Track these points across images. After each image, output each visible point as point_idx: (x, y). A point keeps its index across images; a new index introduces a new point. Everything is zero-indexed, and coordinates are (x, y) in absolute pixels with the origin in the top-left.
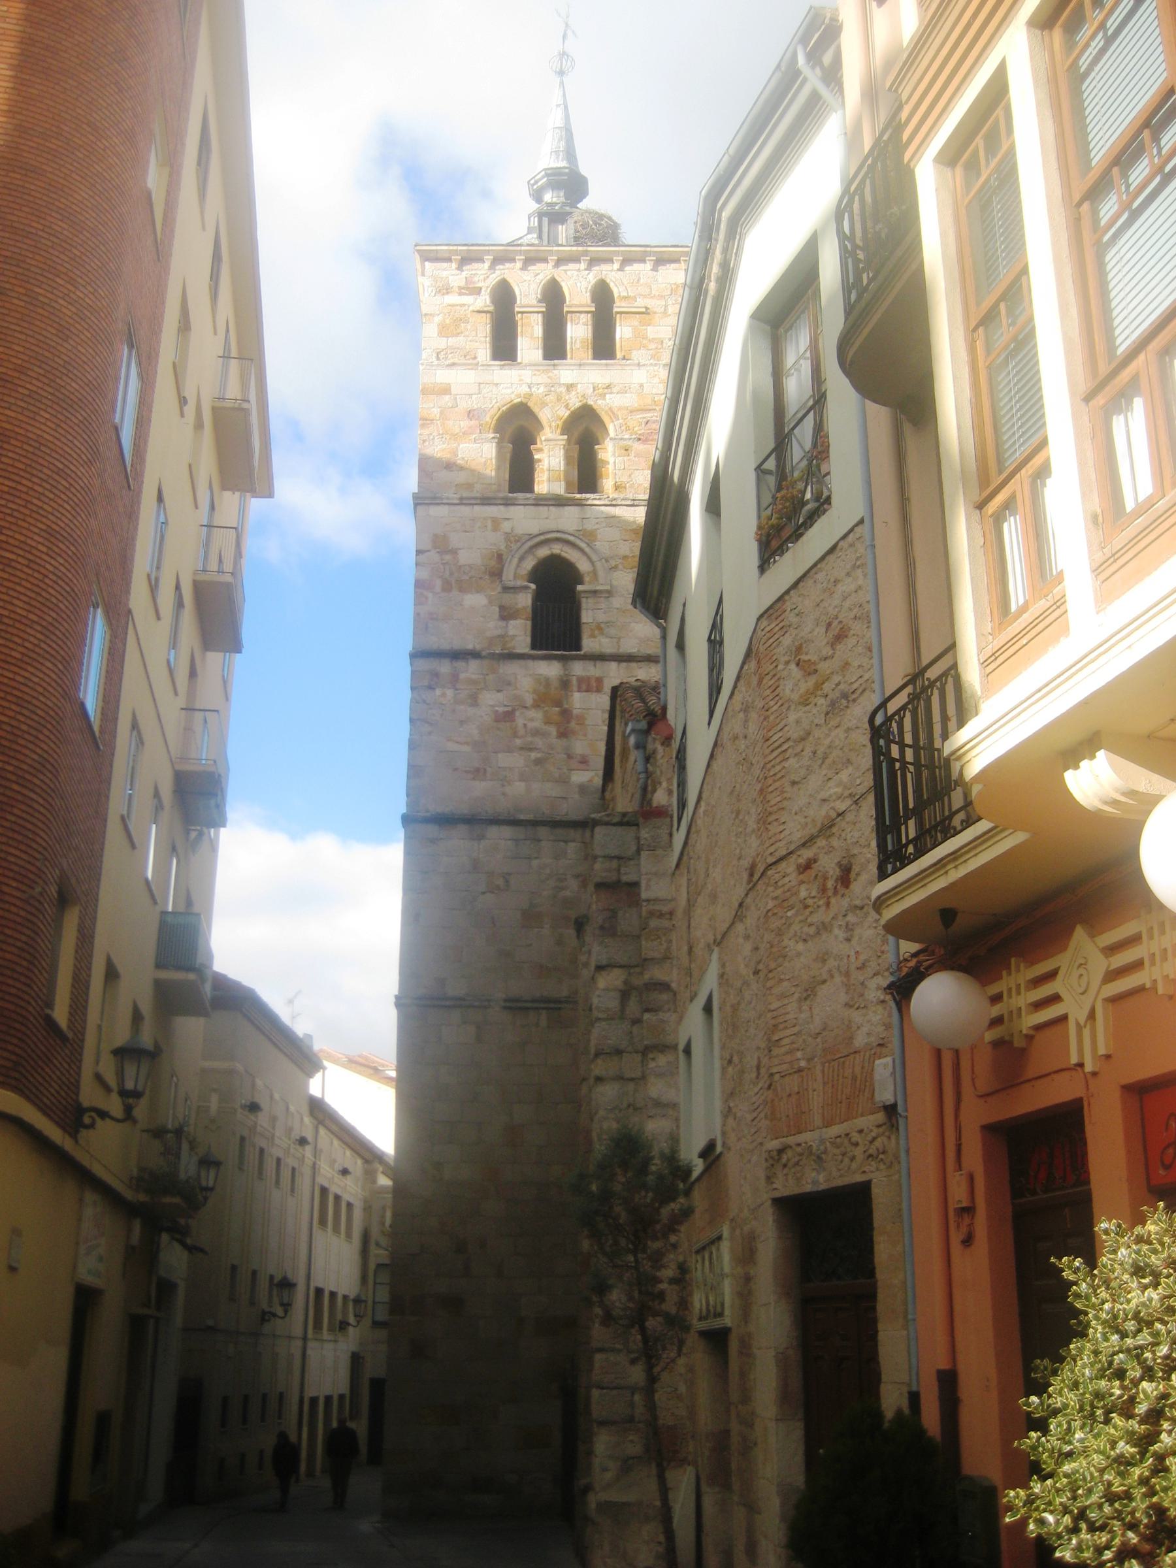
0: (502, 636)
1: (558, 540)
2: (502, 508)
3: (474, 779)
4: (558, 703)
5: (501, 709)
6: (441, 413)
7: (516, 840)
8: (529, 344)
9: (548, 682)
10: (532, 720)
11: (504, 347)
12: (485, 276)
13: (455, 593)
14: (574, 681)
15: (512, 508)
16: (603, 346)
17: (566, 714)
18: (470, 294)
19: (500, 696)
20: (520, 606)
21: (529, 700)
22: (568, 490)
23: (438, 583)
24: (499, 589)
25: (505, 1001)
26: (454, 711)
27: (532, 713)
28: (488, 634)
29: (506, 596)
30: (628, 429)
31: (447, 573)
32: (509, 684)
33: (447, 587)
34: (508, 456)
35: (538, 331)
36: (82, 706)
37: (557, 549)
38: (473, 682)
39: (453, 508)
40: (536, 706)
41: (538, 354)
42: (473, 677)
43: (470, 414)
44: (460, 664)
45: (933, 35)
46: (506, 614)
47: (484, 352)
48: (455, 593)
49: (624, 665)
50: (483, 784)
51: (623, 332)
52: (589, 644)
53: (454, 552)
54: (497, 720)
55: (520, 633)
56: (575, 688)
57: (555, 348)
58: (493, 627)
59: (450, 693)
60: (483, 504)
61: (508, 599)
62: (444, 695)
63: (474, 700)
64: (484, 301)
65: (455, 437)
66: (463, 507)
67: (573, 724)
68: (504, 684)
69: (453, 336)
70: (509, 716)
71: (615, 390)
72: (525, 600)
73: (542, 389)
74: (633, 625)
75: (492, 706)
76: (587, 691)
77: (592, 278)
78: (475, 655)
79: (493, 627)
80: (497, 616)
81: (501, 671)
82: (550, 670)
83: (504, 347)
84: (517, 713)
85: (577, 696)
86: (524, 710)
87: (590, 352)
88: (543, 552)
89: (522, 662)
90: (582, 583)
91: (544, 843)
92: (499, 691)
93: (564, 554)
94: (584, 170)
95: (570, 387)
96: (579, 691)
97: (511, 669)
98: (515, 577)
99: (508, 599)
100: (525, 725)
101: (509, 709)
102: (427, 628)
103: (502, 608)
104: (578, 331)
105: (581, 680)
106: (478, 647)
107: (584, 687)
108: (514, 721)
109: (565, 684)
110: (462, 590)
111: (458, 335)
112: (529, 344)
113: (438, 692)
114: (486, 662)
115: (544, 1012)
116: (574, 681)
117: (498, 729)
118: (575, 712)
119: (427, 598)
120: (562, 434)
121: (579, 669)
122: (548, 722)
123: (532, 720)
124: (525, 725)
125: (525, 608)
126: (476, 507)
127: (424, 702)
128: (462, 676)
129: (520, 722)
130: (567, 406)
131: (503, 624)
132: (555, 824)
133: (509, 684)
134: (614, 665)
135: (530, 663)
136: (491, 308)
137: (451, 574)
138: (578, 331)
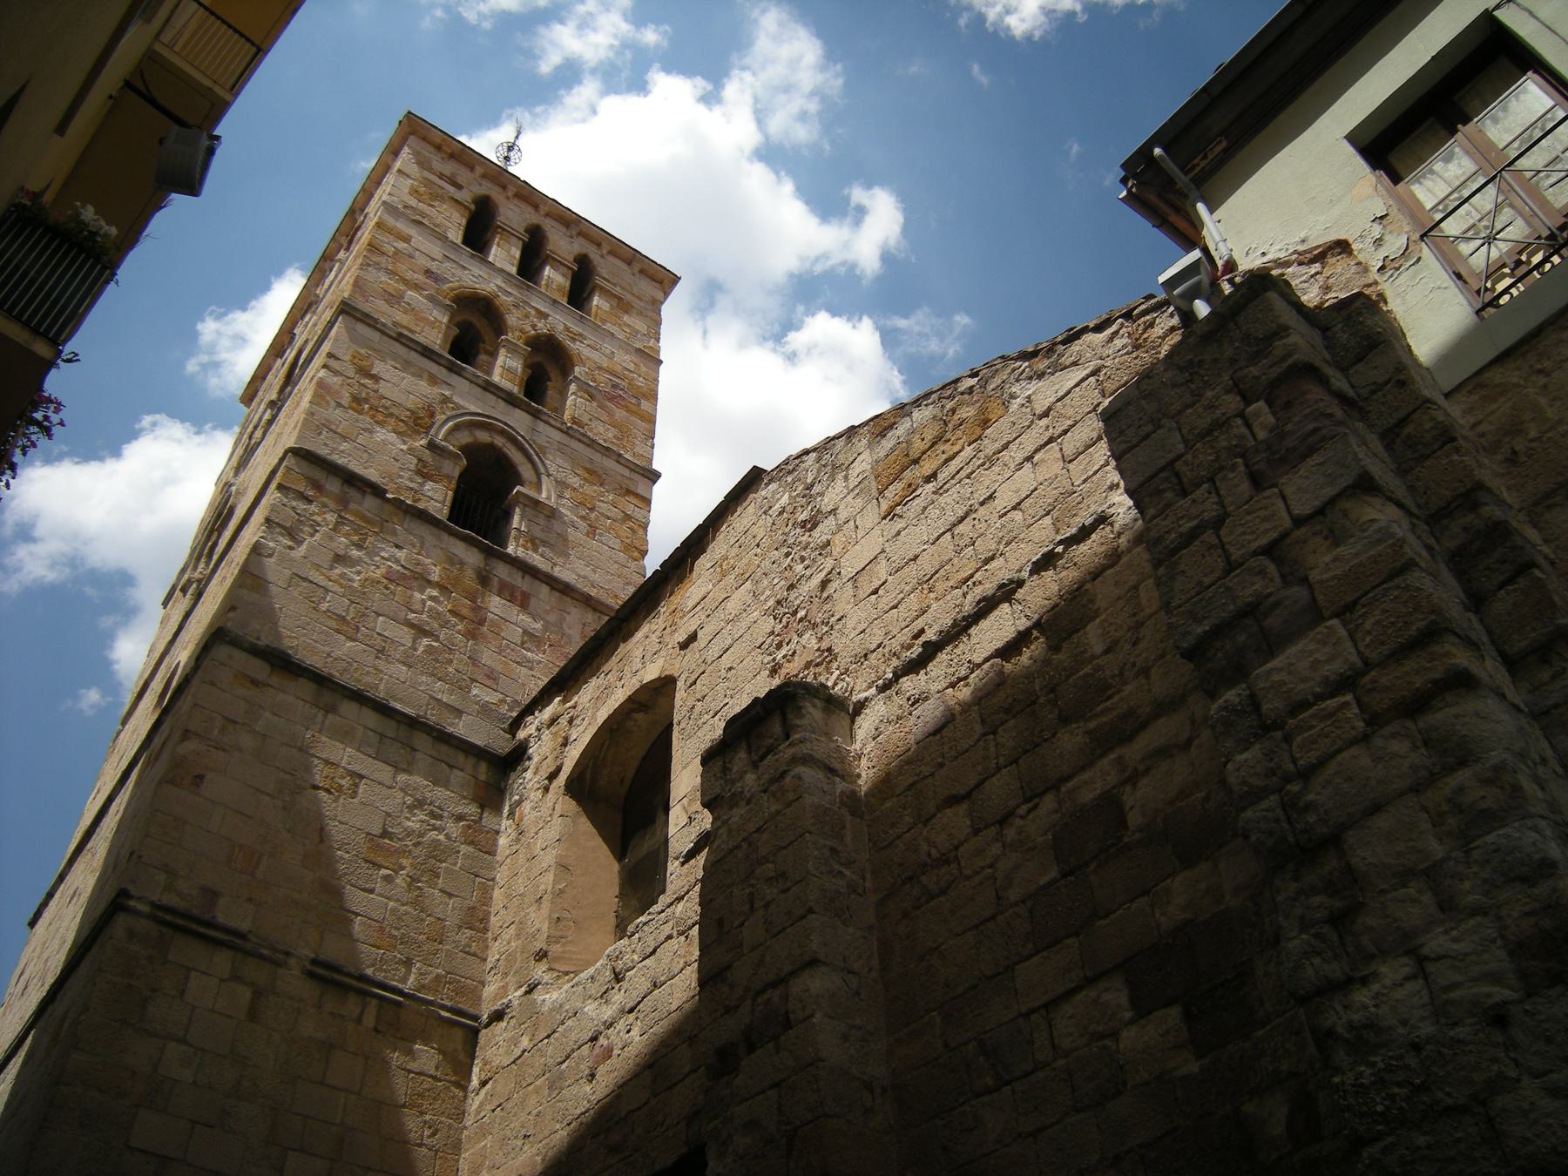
2: (444, 371)
7: (382, 736)
14: (495, 581)
25: (314, 962)
37: (499, 441)
46: (424, 473)
47: (456, 235)
55: (437, 498)
66: (397, 345)
78: (377, 491)
91: (419, 755)
98: (445, 439)
114: (388, 507)
115: (374, 1002)
134: (545, 589)
135: (445, 536)
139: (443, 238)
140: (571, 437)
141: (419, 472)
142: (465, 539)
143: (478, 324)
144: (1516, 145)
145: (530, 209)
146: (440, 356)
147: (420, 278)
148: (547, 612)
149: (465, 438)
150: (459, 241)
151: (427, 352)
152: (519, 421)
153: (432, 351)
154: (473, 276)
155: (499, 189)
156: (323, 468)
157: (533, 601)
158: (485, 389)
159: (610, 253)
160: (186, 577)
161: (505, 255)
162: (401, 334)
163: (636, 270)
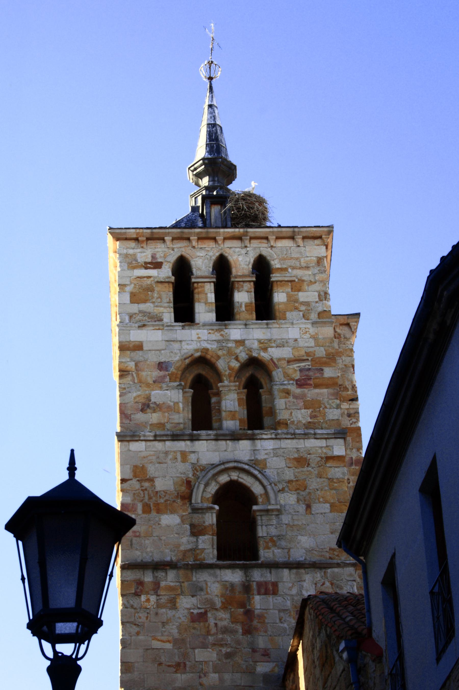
3: (176, 672)
4: (243, 605)
37: (234, 476)
40: (224, 607)
47: (169, 316)
50: (184, 676)
53: (151, 480)
74: (299, 537)
92: (193, 596)
93: (241, 480)
113: (143, 598)
114: (181, 572)
134: (286, 572)
152: (242, 450)
161: (205, 311)
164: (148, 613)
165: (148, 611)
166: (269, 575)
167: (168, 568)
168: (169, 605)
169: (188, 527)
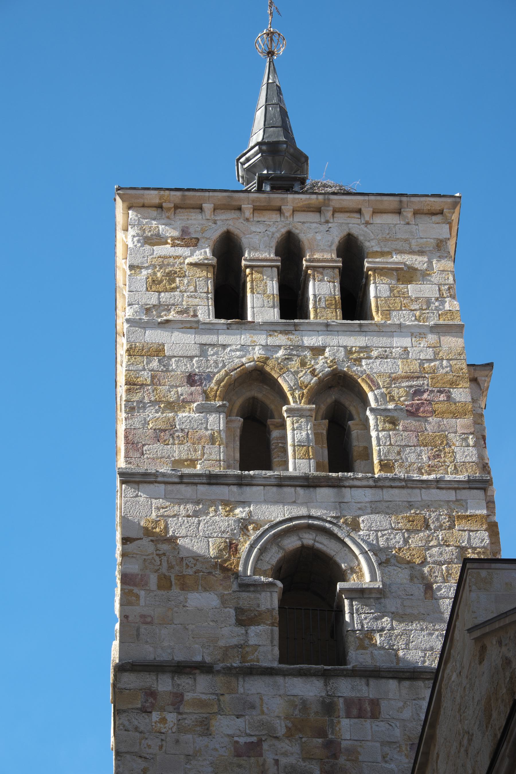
0: (241, 646)
1: (310, 527)
2: (234, 489)
4: (321, 733)
5: (242, 740)
6: (153, 377)
8: (261, 300)
9: (304, 705)
10: (285, 754)
11: (229, 303)
12: (212, 226)
13: (176, 590)
14: (341, 703)
15: (248, 489)
16: (353, 305)
17: (332, 748)
18: (187, 246)
19: (240, 722)
20: (263, 608)
21: (281, 731)
22: (319, 467)
23: (153, 580)
24: (235, 587)
26: (177, 741)
27: (285, 746)
28: (221, 643)
29: (245, 595)
30: (392, 399)
31: (165, 564)
32: (253, 707)
33: (165, 583)
34: (238, 432)
35: (273, 286)
36: (123, 201)
37: (308, 539)
38: (202, 704)
39: (170, 487)
40: (290, 735)
41: (273, 314)
42: (204, 697)
43: (191, 379)
44: (184, 681)
45: (461, 591)
46: (245, 619)
47: (205, 312)
48: (176, 590)
49: (406, 684)
51: (376, 290)
52: (356, 657)
54: (238, 755)
55: (264, 642)
56: (342, 713)
57: (292, 304)
58: (229, 634)
59: (171, 717)
60: (209, 484)
61: (246, 599)
62: (163, 720)
63: (205, 728)
64: (204, 254)
65: (171, 406)
66: (182, 487)
67: (342, 760)
68: (245, 707)
69: (166, 291)
70: (254, 749)
71: (374, 354)
72: (270, 601)
73: (281, 353)
75: (232, 736)
76: (359, 717)
77: (336, 236)
78: (204, 668)
79: (229, 634)
80: (233, 620)
81: (241, 690)
82: (308, 689)
83: (229, 303)
84: (265, 746)
85: (345, 723)
86: (276, 742)
87: (339, 312)
88: (292, 543)
89: (268, 680)
90: (344, 579)
93: (318, 545)
94: (301, 145)
95: (318, 351)
96: (348, 716)
97: (255, 687)
98: (255, 571)
99: (246, 599)
100: (277, 762)
101: (254, 739)
102: (138, 635)
103: (239, 611)
104: (321, 290)
105: (349, 703)
106: (208, 659)
107: (355, 712)
108: (261, 755)
109: (328, 707)
110: (184, 587)
111: (173, 290)
112: (261, 300)
113: (155, 716)
114: (220, 679)
116: (341, 703)
117: (240, 766)
118: (344, 744)
119: (138, 597)
120: (309, 402)
121: (345, 688)
122: (307, 757)
123: (285, 754)
124: (277, 762)
125: (270, 611)
126: (201, 488)
127: (136, 729)
128: (188, 696)
129: (269, 757)
130: (313, 373)
131: (241, 630)
132: (420, 214)
133: (253, 707)
134: (393, 684)
135: (280, 680)
136: (214, 261)
137: (171, 567)
138: (321, 290)
139: (194, 326)
140: (382, 487)
141: (240, 623)
142: (301, 674)
143: (260, 396)
144: (408, 674)
145: (275, 216)
146: (225, 476)
147: (184, 390)
148: (400, 710)
149: (274, 557)
150: (212, 319)
151: (212, 480)
152: (320, 507)
153: (216, 476)
154: (240, 348)
155: (234, 214)
156: (149, 671)
157: (383, 704)
158: (280, 486)
159: (374, 212)
160: (198, 558)
162: (182, 476)
163: (410, 215)
164: (162, 740)
165: (163, 737)
166: (364, 688)
167: (197, 671)
168: (198, 728)
169: (232, 612)
